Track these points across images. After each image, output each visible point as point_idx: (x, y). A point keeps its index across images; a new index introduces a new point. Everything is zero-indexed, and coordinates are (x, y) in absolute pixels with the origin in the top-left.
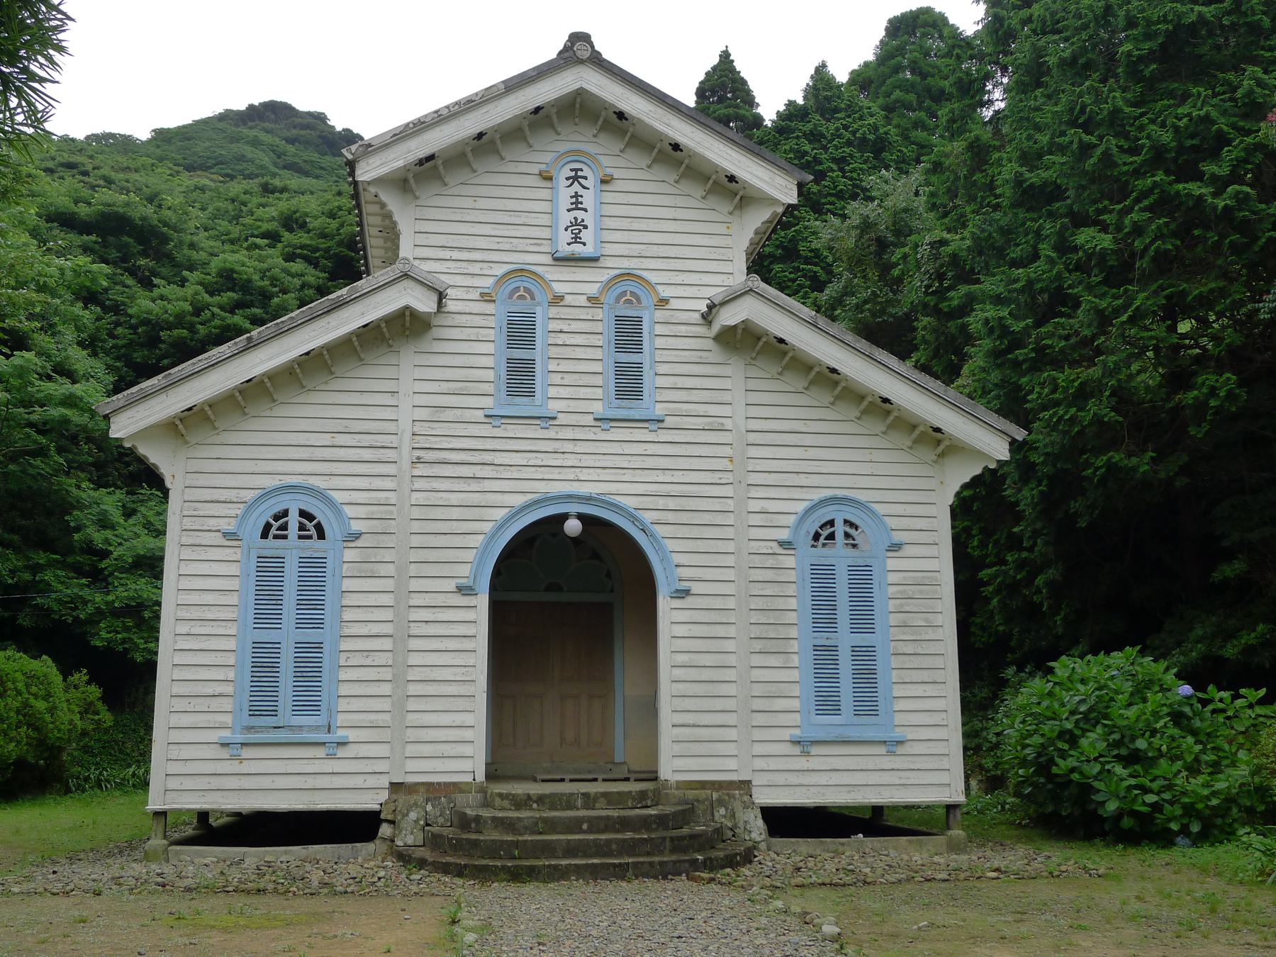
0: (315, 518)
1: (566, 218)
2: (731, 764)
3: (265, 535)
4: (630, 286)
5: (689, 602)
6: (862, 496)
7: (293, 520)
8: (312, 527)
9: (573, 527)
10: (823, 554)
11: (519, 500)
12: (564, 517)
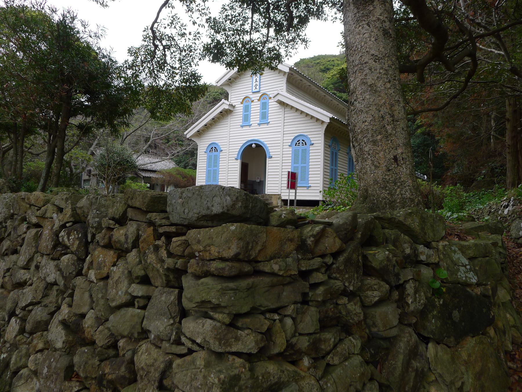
1: (254, 84)
2: (277, 191)
3: (296, 145)
4: (247, 99)
5: (272, 159)
6: (306, 134)
7: (301, 141)
8: (216, 150)
9: (254, 146)
10: (211, 154)
11: (244, 142)
12: (252, 144)
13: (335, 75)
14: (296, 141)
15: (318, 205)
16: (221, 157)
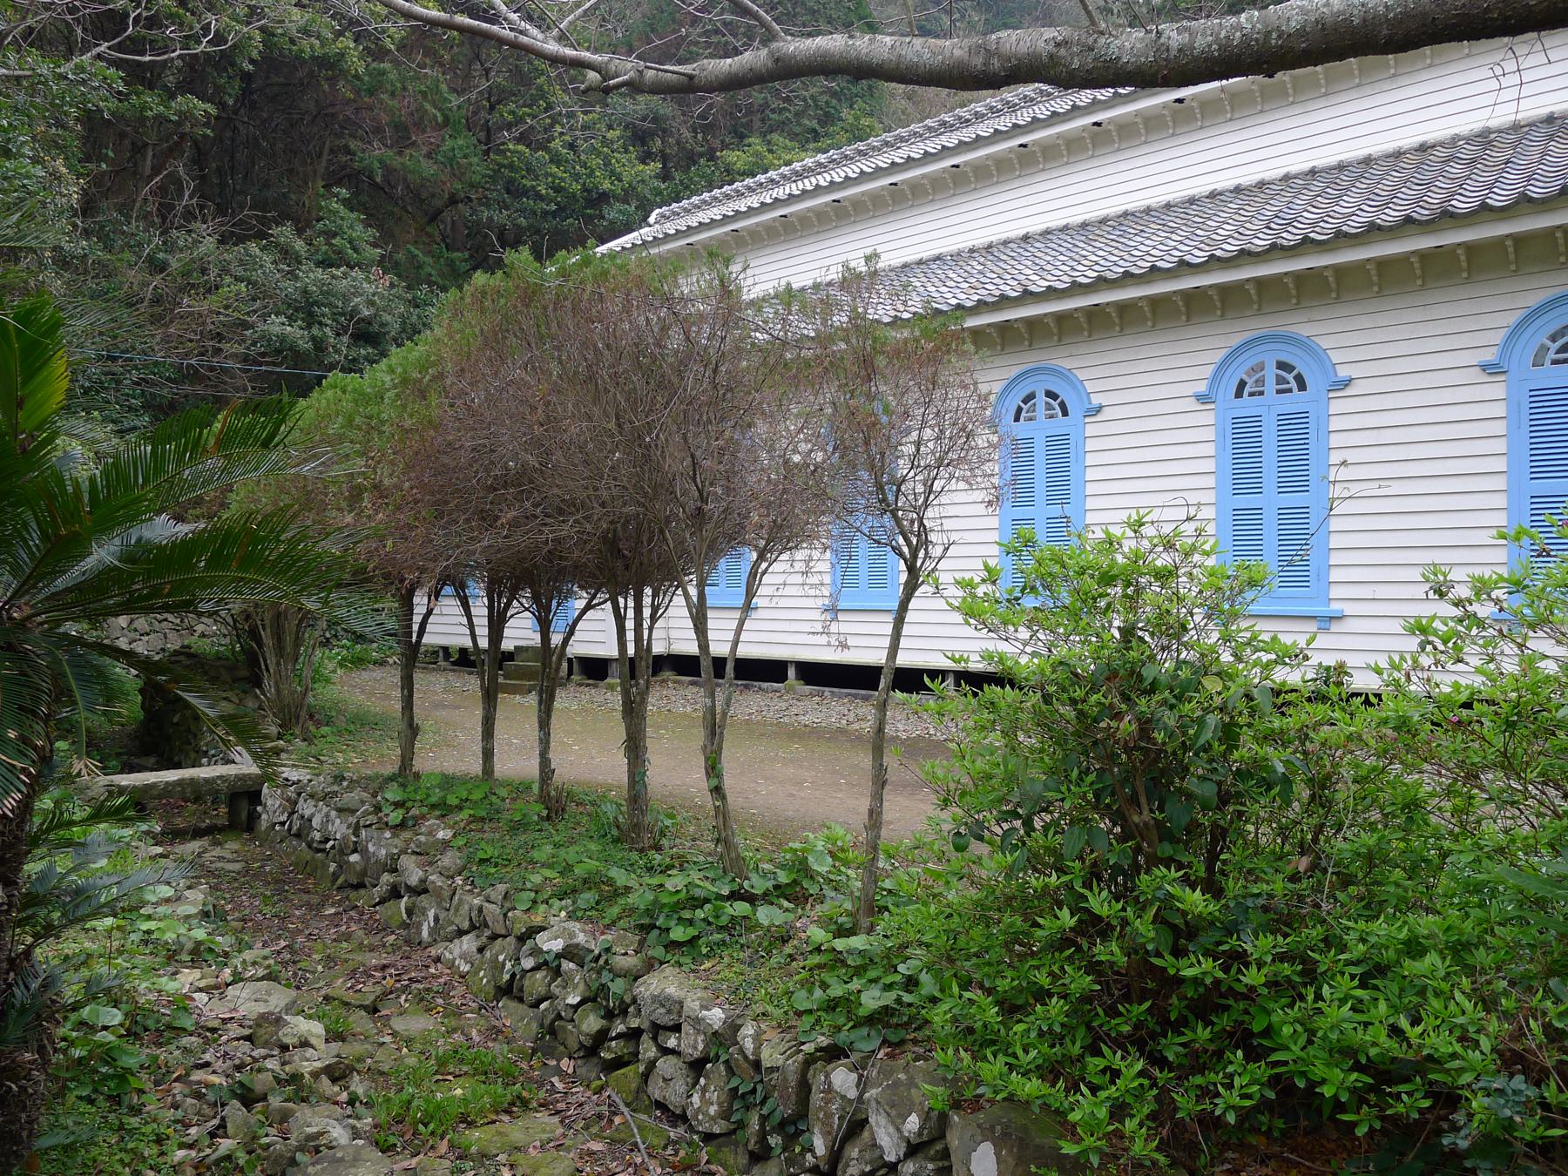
0: (1294, 368)
3: (1239, 394)
10: (1248, 406)
13: (286, 253)
14: (1015, 400)
15: (782, 678)
16: (1335, 424)
